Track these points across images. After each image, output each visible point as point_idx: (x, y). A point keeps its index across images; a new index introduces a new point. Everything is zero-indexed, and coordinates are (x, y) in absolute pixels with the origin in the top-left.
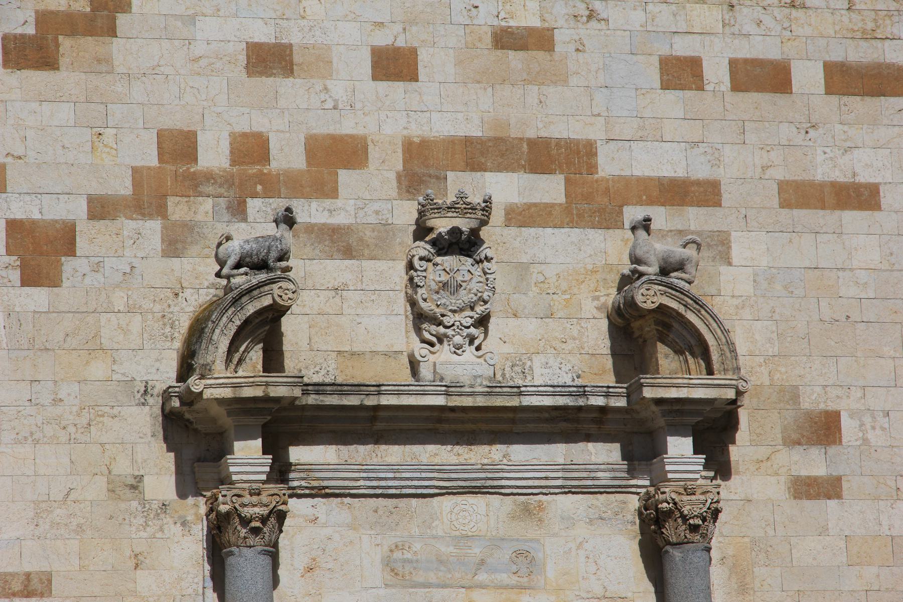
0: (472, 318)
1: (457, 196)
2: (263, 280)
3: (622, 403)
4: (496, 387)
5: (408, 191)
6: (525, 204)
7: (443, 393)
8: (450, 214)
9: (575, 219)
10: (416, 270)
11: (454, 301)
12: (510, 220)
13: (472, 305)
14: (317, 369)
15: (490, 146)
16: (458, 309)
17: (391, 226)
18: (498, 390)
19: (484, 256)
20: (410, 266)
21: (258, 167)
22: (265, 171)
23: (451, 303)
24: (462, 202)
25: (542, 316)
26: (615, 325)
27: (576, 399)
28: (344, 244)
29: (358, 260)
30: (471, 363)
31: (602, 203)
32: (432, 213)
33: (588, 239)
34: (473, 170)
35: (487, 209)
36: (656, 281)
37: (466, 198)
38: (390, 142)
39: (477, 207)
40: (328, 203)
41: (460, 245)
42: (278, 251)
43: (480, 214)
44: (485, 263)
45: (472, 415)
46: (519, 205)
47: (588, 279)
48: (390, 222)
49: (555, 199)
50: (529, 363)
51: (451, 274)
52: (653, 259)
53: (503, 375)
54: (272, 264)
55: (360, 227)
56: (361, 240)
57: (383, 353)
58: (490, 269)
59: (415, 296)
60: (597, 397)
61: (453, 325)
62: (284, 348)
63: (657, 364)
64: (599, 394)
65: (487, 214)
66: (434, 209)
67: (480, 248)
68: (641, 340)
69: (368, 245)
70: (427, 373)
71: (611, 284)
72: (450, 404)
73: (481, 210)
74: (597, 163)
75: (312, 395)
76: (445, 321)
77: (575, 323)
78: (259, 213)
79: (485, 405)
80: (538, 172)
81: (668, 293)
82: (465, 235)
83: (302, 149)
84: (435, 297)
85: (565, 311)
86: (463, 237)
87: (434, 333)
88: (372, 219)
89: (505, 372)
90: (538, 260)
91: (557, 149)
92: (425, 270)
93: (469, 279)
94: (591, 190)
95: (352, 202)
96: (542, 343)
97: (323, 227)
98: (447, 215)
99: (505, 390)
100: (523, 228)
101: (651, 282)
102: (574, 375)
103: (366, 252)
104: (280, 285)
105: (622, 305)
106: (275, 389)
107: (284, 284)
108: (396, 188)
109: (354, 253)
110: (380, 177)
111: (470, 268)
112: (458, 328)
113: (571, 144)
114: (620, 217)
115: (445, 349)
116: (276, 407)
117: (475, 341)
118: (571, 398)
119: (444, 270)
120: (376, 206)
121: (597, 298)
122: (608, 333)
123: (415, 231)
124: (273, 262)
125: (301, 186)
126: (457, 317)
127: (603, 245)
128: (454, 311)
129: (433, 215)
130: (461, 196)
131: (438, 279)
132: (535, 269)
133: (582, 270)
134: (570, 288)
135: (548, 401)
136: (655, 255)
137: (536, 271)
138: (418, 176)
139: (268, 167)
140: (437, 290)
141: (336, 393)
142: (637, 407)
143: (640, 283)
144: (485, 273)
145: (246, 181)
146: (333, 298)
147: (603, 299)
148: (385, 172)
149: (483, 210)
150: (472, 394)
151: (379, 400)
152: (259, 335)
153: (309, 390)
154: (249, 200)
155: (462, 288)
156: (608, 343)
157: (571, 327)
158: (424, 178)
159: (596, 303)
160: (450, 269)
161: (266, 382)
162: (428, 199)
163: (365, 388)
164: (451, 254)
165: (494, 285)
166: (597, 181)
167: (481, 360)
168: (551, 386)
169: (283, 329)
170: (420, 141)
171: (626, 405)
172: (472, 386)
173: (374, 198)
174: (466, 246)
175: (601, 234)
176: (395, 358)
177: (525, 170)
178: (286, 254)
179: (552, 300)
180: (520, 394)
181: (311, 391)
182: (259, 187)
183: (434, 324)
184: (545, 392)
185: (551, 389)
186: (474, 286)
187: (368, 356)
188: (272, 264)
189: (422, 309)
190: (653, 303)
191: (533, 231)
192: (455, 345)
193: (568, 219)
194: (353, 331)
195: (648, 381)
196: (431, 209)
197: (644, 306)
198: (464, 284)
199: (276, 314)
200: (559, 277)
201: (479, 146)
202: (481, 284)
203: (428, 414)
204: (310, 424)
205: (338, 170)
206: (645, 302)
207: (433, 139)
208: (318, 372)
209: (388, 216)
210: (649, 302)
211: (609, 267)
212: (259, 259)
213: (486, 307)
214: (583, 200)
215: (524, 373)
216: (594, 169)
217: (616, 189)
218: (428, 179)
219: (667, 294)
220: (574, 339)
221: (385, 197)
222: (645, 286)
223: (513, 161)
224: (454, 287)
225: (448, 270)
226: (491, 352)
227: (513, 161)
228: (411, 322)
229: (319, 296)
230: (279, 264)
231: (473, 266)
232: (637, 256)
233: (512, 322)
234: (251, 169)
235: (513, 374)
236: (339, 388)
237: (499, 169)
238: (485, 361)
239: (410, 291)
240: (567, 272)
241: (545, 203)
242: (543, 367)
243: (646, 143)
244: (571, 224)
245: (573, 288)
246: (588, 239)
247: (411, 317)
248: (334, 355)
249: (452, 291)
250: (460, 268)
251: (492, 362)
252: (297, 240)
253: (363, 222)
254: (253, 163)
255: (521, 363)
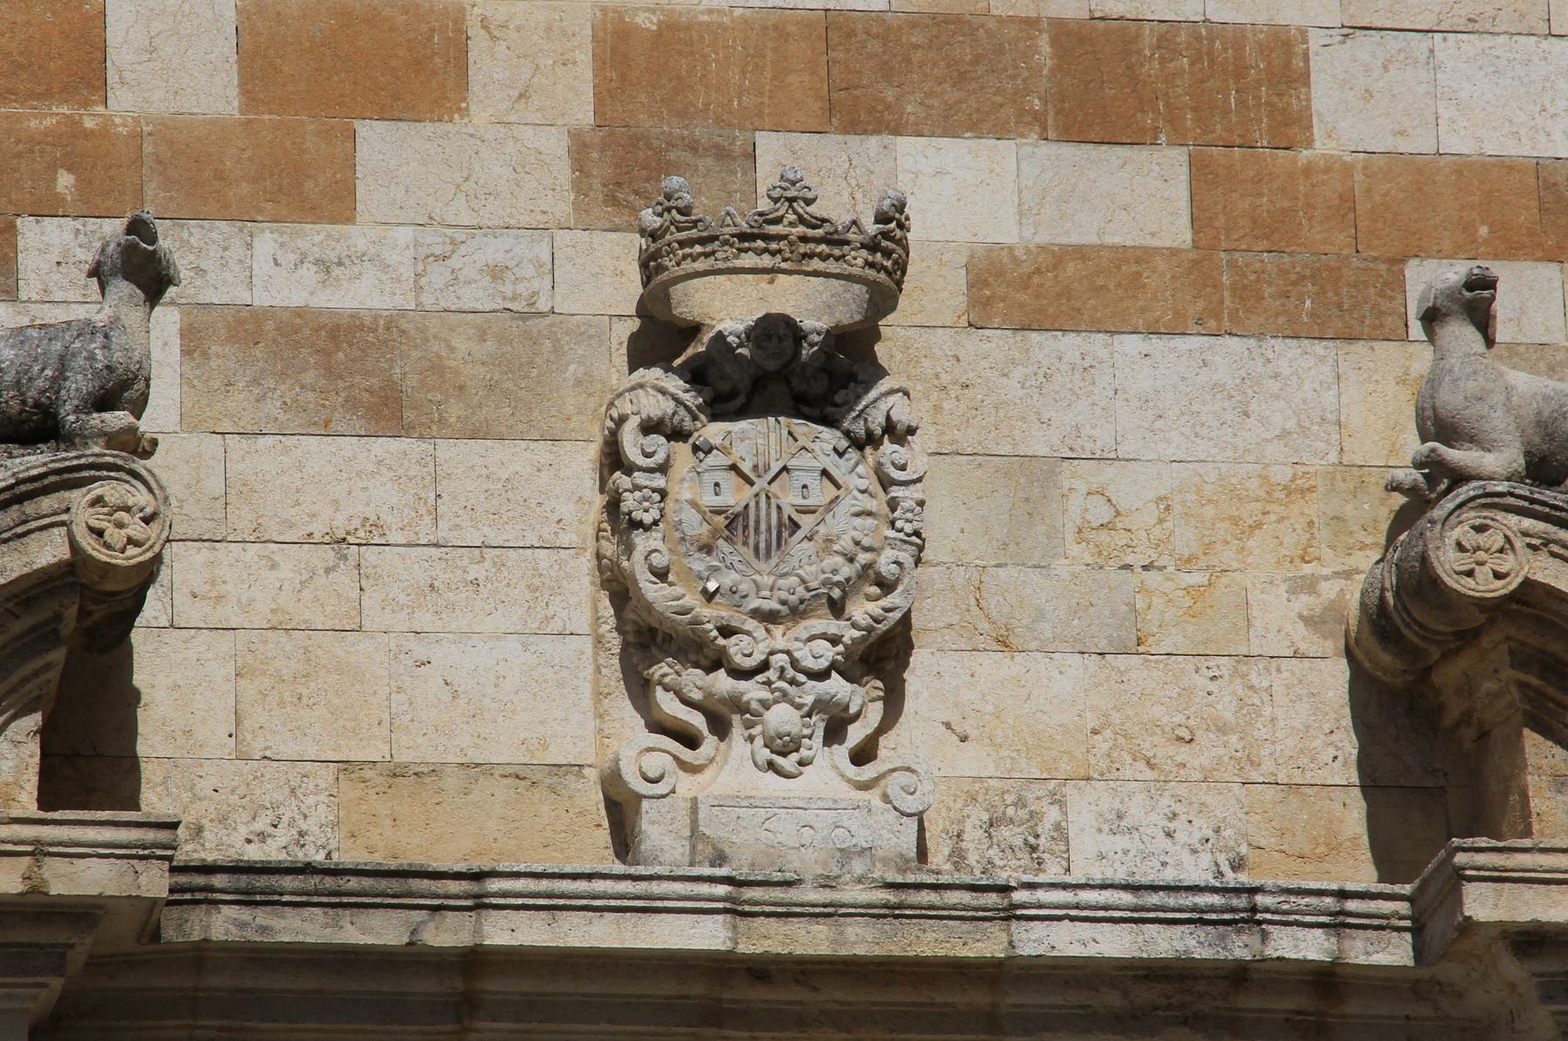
0: (834, 640)
1: (776, 194)
2: (34, 472)
3: (1395, 952)
4: (919, 887)
5: (611, 200)
6: (1042, 248)
7: (720, 905)
8: (748, 260)
9: (1227, 303)
10: (629, 469)
11: (767, 580)
12: (987, 303)
13: (836, 594)
14: (262, 824)
15: (916, 47)
16: (784, 610)
17: (547, 321)
18: (926, 897)
19: (882, 420)
20: (613, 459)
21: (65, 110)
22: (89, 124)
23: (758, 587)
24: (792, 217)
25: (1103, 645)
26: (1373, 680)
27: (1223, 938)
28: (374, 381)
29: (421, 437)
30: (830, 804)
31: (1328, 249)
32: (685, 257)
33: (1276, 376)
34: (853, 126)
35: (885, 243)
36: (1511, 500)
37: (808, 202)
38: (549, 29)
39: (851, 236)
40: (317, 239)
41: (795, 382)
42: (96, 373)
43: (860, 261)
44: (888, 447)
45: (833, 995)
46: (1019, 253)
47: (1273, 517)
48: (543, 305)
49: (1153, 234)
50: (1053, 814)
51: (761, 484)
52: (1499, 422)
53: (958, 857)
54: (72, 418)
55: (433, 323)
56: (436, 367)
57: (509, 770)
58: (903, 468)
59: (625, 564)
60: (1301, 933)
61: (764, 666)
62: (142, 749)
63: (1526, 814)
64: (1308, 919)
65: (888, 264)
66: (691, 242)
67: (867, 390)
68: (1469, 734)
69: (461, 388)
70: (667, 841)
71: (1361, 536)
72: (745, 948)
73: (863, 246)
74: (1309, 108)
75: (225, 909)
76: (732, 651)
77: (1225, 671)
78: (63, 269)
79: (877, 951)
80: (1092, 137)
81: (1554, 542)
82: (812, 345)
83: (227, 47)
84: (699, 564)
85: (1190, 629)
86: (806, 352)
87: (697, 696)
88: (477, 296)
89: (964, 845)
90: (1089, 446)
91: (1162, 60)
92: (663, 469)
93: (825, 500)
94: (1286, 204)
95: (405, 234)
96: (1102, 744)
97: (298, 321)
98: (738, 263)
99: (953, 897)
100: (1034, 334)
101: (1491, 501)
102: (1222, 859)
103: (454, 411)
104: (99, 492)
105: (1389, 596)
106: (70, 869)
107: (112, 491)
108: (568, 186)
109: (409, 415)
110: (510, 147)
111: (830, 462)
112: (781, 677)
113: (1212, 40)
114: (1392, 298)
115: (733, 761)
116: (83, 946)
117: (851, 728)
118: (1201, 932)
119: (734, 468)
120: (493, 250)
121: (1309, 585)
122: (1347, 711)
123: (634, 339)
124: (77, 410)
125: (220, 176)
126: (780, 637)
127: (1329, 397)
128: (768, 618)
129: (688, 266)
130: (792, 195)
131: (710, 500)
132: (1077, 479)
133: (1253, 485)
134: (1208, 548)
135: (1114, 943)
136: (1508, 408)
137: (1082, 487)
138: (649, 146)
139: (100, 109)
140: (705, 539)
141: (316, 899)
142: (1450, 971)
143: (1451, 506)
144: (886, 483)
145: (18, 155)
146: (328, 571)
147: (1329, 590)
148: (529, 131)
149: (872, 246)
150: (828, 912)
151: (477, 931)
152: (26, 680)
153: (212, 889)
154: (25, 224)
155: (800, 534)
156: (1349, 745)
157: (1212, 686)
158: (672, 156)
159: (1303, 602)
160: (755, 467)
161: (36, 842)
162: (669, 210)
163: (425, 884)
164: (762, 413)
165: (916, 525)
166: (1308, 171)
167: (873, 797)
168: (1126, 887)
169: (139, 679)
170: (659, 24)
171: (1411, 963)
172: (827, 883)
173: (484, 222)
174: (818, 387)
175: (1322, 359)
176: (553, 790)
177: (1044, 128)
178: (126, 384)
179: (1142, 589)
180: (1010, 914)
181: (222, 891)
182: (65, 180)
183: (696, 665)
184: (1105, 908)
185: (1127, 898)
186: (844, 527)
187: (451, 781)
188: (72, 418)
189: (649, 607)
190: (1498, 576)
191: (1069, 343)
192: (772, 739)
193: (1201, 304)
194: (400, 690)
195: (1481, 859)
196: (682, 244)
197: (1465, 586)
198: (806, 522)
199: (99, 613)
200: (1168, 508)
201: (875, 46)
202: (870, 521)
203: (667, 988)
204: (225, 1022)
205: (357, 124)
206: (1470, 573)
207: (705, 18)
208: (262, 836)
209: (536, 284)
210: (1484, 573)
211: (1349, 473)
212: (24, 402)
213: (887, 602)
214: (1256, 237)
215: (1034, 849)
216: (1296, 129)
217: (1378, 198)
218: (687, 156)
219: (1555, 548)
220: (1223, 729)
221: (525, 220)
222: (1472, 516)
223: (999, 99)
224: (769, 530)
225: (746, 467)
226: (909, 769)
227: (999, 99)
228: (616, 661)
229: (274, 566)
230: (96, 419)
231: (841, 454)
232: (1443, 413)
233: (993, 666)
234: (35, 117)
235: (991, 852)
236: (329, 882)
237: (948, 125)
238: (886, 798)
239: (609, 548)
240: (1199, 490)
241: (1114, 248)
242: (1106, 828)
243: (1488, 41)
244: (1212, 323)
245: (1218, 547)
246: (1276, 376)
247: (615, 642)
248: (326, 775)
249: (762, 545)
250: (792, 463)
251: (910, 804)
252: (198, 366)
253: (443, 304)
254: (47, 95)
255: (1023, 814)
